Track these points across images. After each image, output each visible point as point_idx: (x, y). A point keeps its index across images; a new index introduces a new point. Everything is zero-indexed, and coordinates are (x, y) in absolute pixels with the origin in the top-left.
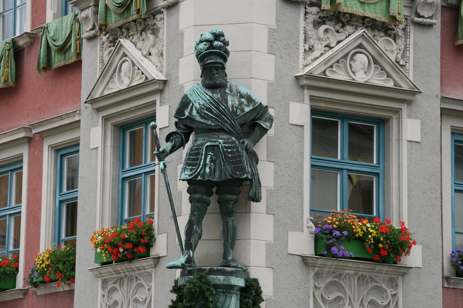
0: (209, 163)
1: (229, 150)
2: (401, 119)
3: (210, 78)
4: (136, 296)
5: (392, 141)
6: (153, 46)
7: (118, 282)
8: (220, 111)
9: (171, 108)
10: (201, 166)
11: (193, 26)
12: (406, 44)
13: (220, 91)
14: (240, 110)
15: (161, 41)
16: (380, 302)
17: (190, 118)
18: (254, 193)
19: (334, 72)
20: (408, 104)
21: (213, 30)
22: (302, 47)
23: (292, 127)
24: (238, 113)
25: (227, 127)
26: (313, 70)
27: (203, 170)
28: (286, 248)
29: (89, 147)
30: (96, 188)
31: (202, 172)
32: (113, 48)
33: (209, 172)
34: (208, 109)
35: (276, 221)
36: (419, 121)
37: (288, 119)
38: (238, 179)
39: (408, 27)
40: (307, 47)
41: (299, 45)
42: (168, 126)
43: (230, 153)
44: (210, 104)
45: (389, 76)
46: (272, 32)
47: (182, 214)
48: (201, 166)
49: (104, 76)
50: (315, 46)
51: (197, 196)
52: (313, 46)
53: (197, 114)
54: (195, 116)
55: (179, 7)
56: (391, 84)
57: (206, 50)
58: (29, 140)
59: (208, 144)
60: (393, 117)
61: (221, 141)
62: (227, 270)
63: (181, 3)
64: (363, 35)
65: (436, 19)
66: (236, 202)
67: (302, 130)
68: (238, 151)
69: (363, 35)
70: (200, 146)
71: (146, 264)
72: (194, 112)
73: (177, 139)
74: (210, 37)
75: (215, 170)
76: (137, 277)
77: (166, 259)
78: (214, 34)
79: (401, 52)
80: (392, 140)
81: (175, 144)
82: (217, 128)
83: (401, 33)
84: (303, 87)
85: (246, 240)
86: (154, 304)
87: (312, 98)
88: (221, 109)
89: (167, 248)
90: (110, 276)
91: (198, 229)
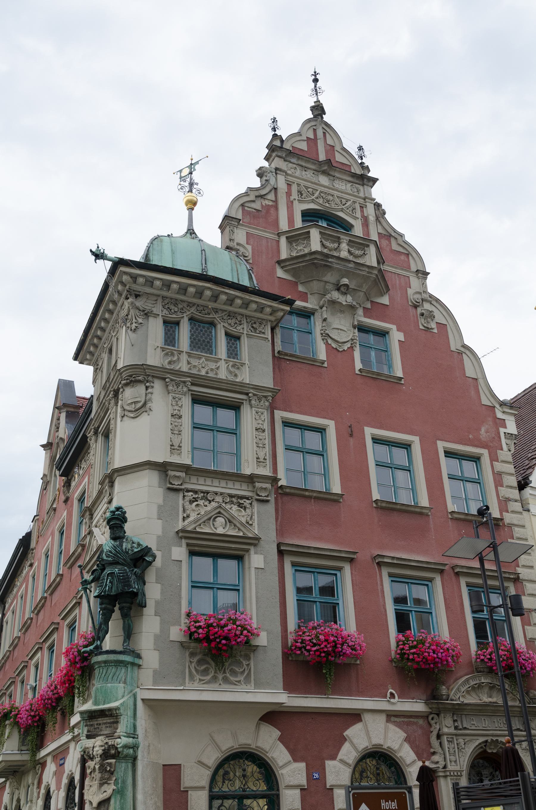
13: (119, 541)
14: (131, 550)
16: (238, 670)
19: (202, 528)
20: (254, 546)
23: (174, 562)
24: (129, 552)
28: (169, 637)
34: (110, 552)
35: (161, 620)
36: (262, 556)
37: (171, 558)
40: (185, 515)
41: (178, 514)
43: (122, 576)
45: (239, 529)
46: (160, 507)
51: (103, 606)
56: (241, 534)
61: (117, 570)
65: (271, 497)
68: (127, 575)
75: (112, 588)
79: (250, 517)
82: (114, 562)
83: (248, 506)
87: (188, 545)
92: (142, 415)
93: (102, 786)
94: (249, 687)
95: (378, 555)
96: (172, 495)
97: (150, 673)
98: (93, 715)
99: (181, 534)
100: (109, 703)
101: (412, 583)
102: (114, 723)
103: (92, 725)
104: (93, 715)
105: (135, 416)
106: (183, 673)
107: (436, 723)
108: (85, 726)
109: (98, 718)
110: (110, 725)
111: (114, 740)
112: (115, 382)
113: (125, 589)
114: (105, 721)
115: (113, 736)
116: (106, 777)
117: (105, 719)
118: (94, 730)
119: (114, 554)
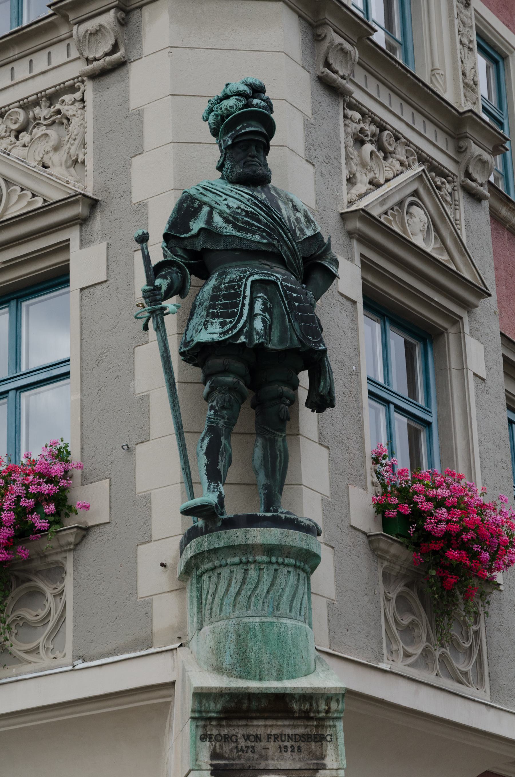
0: (261, 313)
1: (294, 295)
2: (462, 335)
3: (244, 164)
5: (450, 371)
8: (274, 219)
9: (110, 249)
11: (170, 96)
15: (75, 139)
18: (329, 388)
21: (248, 79)
25: (285, 252)
26: (371, 206)
31: (246, 328)
33: (263, 328)
39: (456, 193)
42: (106, 281)
44: (253, 207)
47: (151, 438)
48: (244, 318)
52: (354, 175)
53: (224, 225)
54: (221, 227)
55: (128, 71)
57: (240, 109)
59: (256, 277)
60: (450, 330)
62: (302, 522)
63: (133, 64)
64: (421, 175)
67: (353, 309)
69: (421, 175)
70: (238, 281)
72: (218, 220)
73: (175, 275)
74: (248, 91)
77: (105, 530)
80: (450, 368)
81: (172, 281)
82: (270, 250)
85: (292, 486)
88: (275, 216)
89: (111, 508)
91: (227, 444)
98: (245, 706)
99: (357, 224)
100: (293, 677)
102: (306, 738)
103: (227, 738)
104: (245, 706)
108: (204, 738)
114: (274, 732)
117: (280, 723)
118: (235, 754)
119: (265, 225)
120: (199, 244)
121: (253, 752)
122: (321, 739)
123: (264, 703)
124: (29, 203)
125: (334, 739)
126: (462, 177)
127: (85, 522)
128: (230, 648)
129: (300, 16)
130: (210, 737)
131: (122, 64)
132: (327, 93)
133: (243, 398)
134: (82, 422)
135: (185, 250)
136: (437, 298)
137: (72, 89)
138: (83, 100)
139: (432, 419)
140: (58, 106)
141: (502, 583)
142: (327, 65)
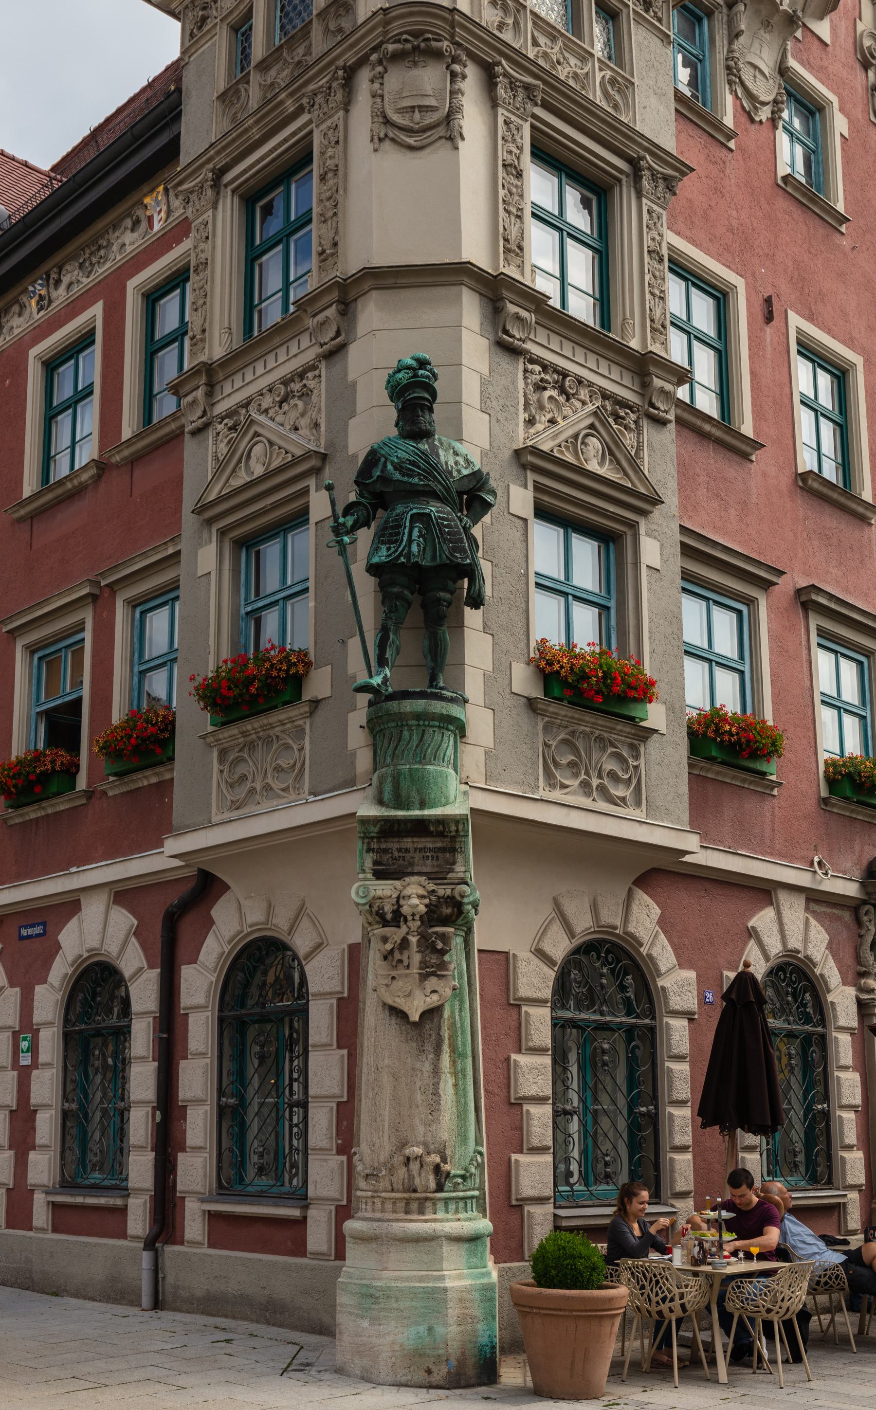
1: (445, 523)
4: (278, 762)
6: (302, 415)
7: (246, 748)
10: (404, 543)
12: (638, 442)
17: (384, 479)
22: (523, 416)
27: (407, 549)
29: (196, 574)
30: (208, 626)
32: (236, 435)
34: (412, 463)
38: (459, 564)
48: (404, 543)
49: (223, 470)
50: (537, 417)
52: (534, 417)
58: (93, 598)
59: (415, 511)
61: (433, 509)
66: (449, 604)
71: (296, 712)
72: (390, 467)
74: (414, 363)
76: (277, 737)
78: (418, 360)
81: (358, 518)
82: (428, 489)
84: (524, 467)
86: (310, 767)
90: (232, 743)
92: (438, 144)
93: (426, 980)
94: (638, 811)
95: (813, 586)
96: (504, 361)
97: (480, 754)
101: (843, 655)
102: (443, 850)
104: (396, 828)
105: (419, 144)
106: (535, 764)
107: (870, 921)
108: (369, 850)
109: (403, 837)
110: (435, 855)
111: (453, 886)
112: (352, 46)
113: (457, 558)
115: (446, 879)
116: (434, 961)
117: (423, 840)
120: (379, 487)
121: (404, 860)
122: (453, 850)
123: (409, 825)
124: (283, 459)
125: (464, 851)
126: (646, 407)
127: (316, 697)
128: (388, 788)
129: (481, 294)
130: (373, 850)
131: (343, 347)
132: (507, 354)
133: (409, 604)
134: (315, 623)
135: (370, 492)
136: (612, 508)
137: (314, 368)
138: (320, 376)
139: (612, 604)
140: (304, 382)
141: (663, 730)
142: (506, 332)
